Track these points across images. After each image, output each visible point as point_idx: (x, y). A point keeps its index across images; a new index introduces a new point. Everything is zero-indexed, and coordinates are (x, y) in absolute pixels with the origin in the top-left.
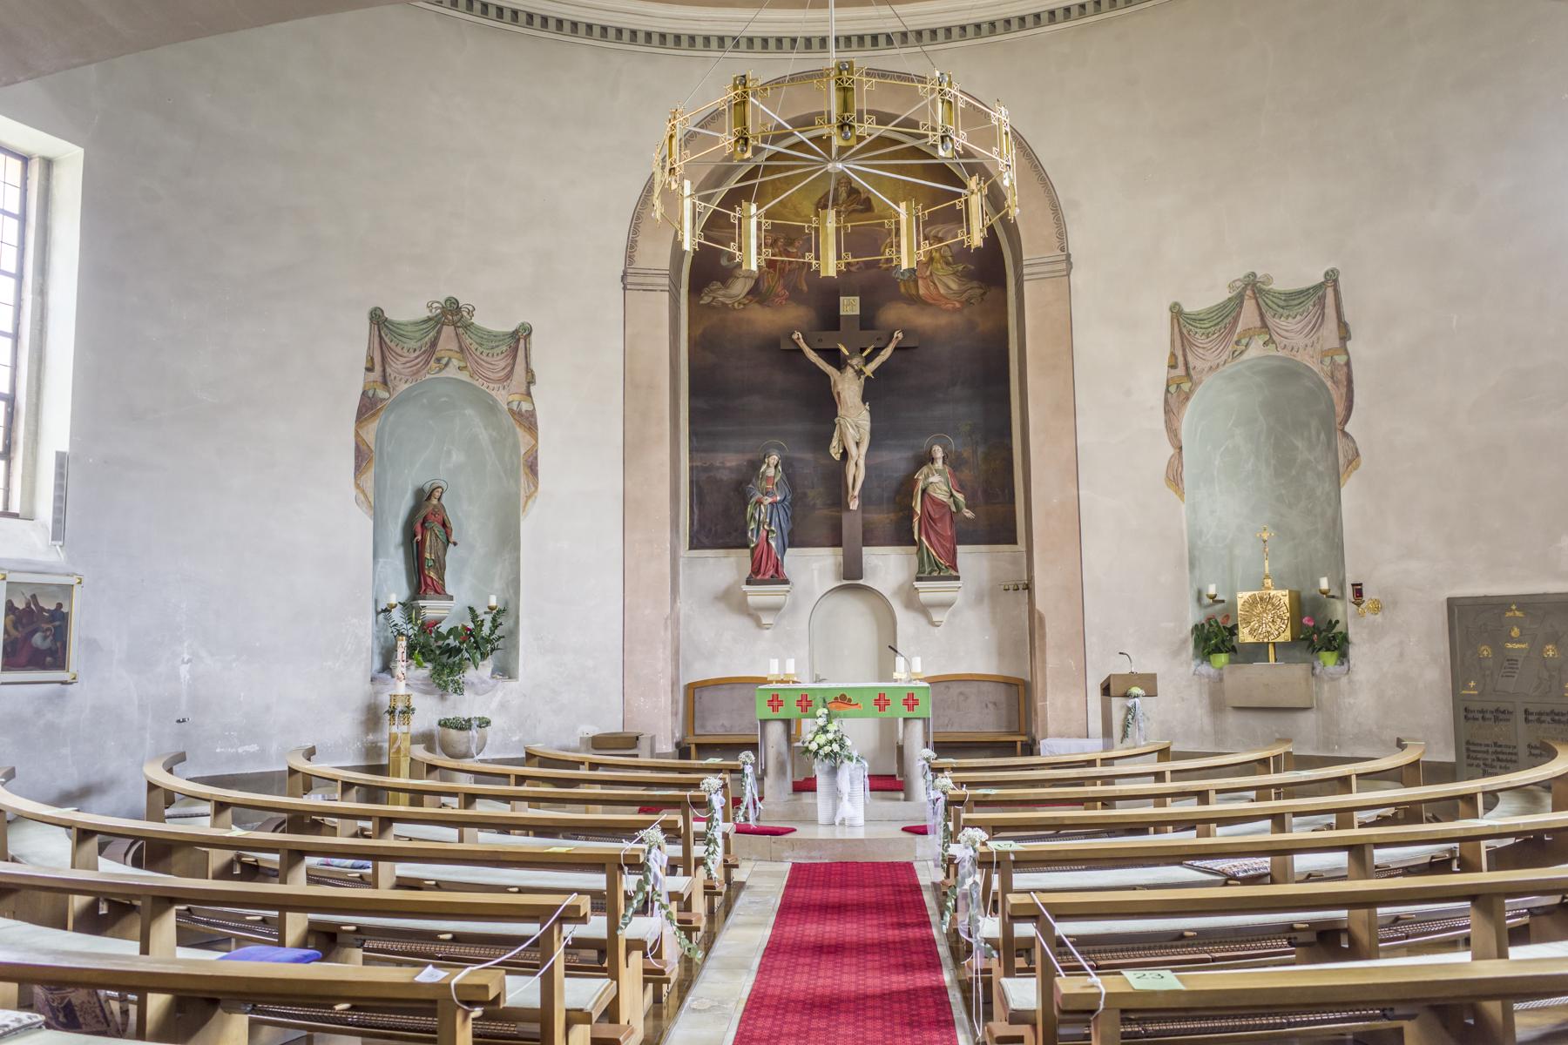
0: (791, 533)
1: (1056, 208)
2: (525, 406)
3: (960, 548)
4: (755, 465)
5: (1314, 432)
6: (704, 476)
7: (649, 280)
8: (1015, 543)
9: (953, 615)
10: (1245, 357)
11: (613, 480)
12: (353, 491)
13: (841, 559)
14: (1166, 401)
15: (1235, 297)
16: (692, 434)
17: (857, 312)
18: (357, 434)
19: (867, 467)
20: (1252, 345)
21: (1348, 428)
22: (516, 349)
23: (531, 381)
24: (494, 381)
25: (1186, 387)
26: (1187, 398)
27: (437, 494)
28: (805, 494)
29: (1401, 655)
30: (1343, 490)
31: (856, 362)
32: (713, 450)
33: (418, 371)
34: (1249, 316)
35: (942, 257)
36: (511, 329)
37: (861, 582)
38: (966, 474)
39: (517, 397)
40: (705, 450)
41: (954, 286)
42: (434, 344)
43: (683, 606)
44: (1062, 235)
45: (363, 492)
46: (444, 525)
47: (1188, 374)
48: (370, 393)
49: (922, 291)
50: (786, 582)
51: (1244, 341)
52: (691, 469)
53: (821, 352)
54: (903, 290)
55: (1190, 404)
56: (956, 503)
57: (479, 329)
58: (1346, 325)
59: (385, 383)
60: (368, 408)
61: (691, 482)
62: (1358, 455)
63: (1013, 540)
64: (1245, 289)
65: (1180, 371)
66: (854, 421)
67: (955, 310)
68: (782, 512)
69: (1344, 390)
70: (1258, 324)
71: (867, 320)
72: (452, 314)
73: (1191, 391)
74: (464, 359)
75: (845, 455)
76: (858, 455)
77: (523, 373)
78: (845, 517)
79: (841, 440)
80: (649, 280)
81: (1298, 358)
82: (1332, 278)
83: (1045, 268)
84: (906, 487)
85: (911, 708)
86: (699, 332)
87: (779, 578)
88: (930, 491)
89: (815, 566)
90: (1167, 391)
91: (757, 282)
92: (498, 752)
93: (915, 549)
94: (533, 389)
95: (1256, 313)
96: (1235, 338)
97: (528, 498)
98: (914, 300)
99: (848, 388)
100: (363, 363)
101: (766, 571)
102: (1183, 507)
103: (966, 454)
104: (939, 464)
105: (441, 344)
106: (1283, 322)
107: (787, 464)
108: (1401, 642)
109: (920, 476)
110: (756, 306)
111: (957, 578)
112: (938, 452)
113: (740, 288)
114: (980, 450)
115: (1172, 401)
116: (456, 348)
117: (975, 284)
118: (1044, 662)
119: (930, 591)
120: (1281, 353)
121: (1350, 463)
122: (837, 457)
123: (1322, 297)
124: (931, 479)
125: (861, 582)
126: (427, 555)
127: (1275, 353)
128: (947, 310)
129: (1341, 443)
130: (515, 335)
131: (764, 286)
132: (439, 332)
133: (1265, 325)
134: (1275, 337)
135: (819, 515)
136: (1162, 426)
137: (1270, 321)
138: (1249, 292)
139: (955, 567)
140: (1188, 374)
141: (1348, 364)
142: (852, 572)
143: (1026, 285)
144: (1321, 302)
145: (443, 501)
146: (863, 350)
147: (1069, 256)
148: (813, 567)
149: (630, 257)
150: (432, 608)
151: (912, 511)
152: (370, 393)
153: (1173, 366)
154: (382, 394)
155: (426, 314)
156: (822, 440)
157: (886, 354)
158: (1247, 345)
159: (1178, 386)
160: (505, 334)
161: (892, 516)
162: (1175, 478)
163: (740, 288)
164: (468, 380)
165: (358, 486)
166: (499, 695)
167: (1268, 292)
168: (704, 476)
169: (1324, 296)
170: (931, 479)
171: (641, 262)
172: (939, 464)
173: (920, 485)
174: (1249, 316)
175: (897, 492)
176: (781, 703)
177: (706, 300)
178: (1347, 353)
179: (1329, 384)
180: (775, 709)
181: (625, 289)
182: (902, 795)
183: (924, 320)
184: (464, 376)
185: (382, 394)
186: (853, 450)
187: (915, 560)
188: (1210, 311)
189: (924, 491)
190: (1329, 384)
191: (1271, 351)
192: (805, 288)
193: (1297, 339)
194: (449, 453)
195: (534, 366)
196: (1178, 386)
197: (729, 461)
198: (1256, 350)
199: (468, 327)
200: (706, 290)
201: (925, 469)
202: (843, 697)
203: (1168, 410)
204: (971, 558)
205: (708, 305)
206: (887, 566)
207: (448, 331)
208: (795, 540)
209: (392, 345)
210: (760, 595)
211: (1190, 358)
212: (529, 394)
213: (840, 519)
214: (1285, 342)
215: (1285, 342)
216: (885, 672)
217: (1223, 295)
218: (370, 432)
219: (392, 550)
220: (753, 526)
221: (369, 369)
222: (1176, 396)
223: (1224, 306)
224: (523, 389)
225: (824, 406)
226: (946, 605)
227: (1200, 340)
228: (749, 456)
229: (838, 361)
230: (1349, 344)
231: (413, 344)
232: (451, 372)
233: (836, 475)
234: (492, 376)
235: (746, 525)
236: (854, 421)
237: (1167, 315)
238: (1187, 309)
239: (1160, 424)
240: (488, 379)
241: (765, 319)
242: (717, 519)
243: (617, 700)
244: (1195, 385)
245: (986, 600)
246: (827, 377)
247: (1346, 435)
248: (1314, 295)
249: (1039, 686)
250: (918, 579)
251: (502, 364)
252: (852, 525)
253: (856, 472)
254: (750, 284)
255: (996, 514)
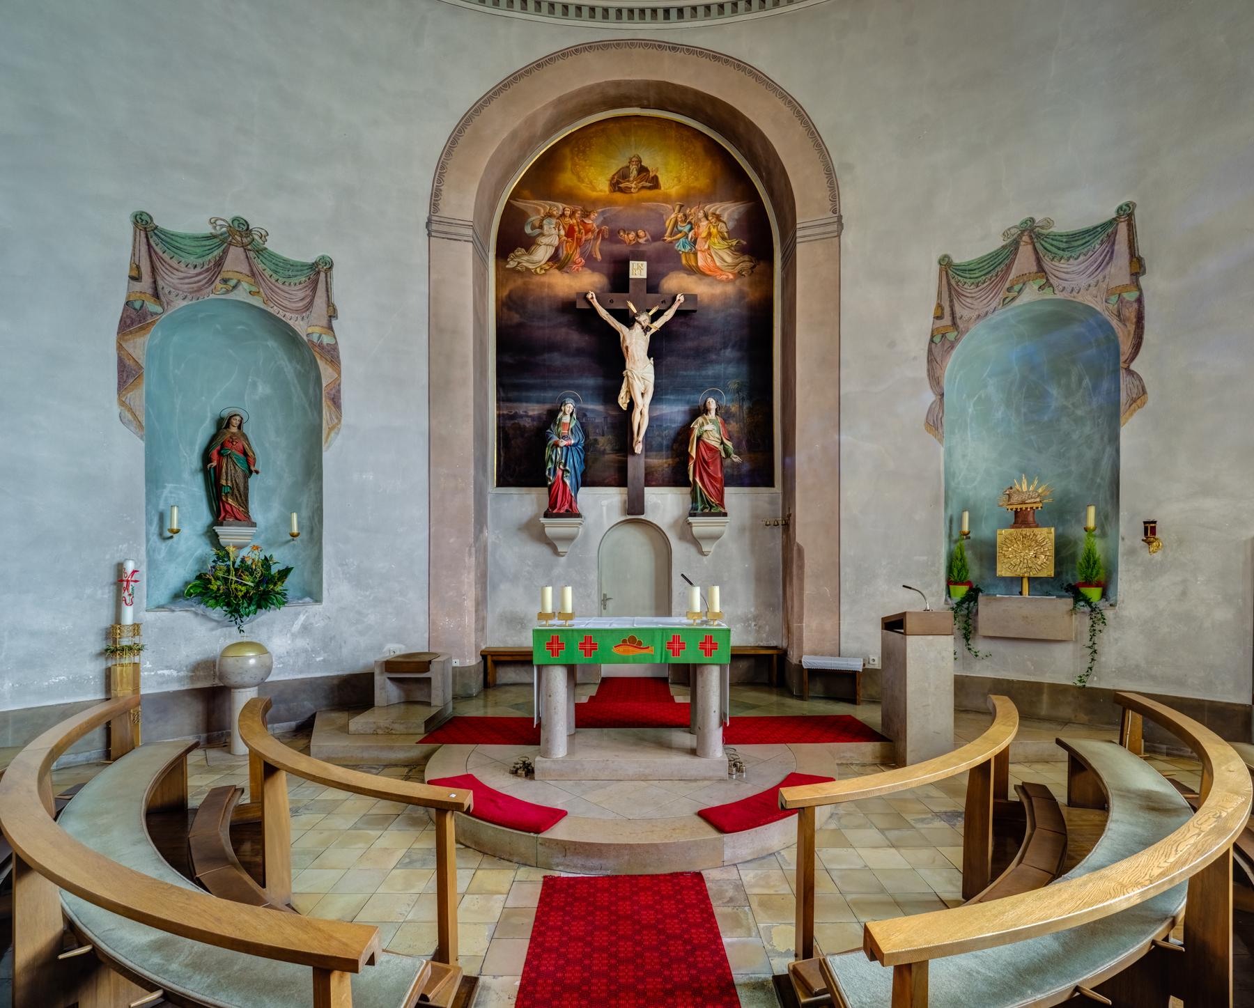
0: (584, 474)
1: (830, 172)
2: (327, 340)
3: (727, 490)
4: (552, 416)
5: (1074, 379)
6: (509, 423)
7: (453, 229)
8: (773, 486)
9: (719, 546)
10: (1017, 302)
11: (422, 422)
12: (116, 409)
13: (625, 497)
14: (930, 351)
15: (1010, 245)
16: (500, 385)
17: (645, 276)
18: (120, 347)
19: (651, 419)
20: (1027, 290)
21: (1133, 367)
22: (316, 282)
23: (332, 314)
24: (291, 310)
25: (951, 336)
26: (952, 347)
27: (235, 422)
28: (596, 440)
29: (1184, 593)
30: (1125, 432)
31: (644, 319)
32: (519, 400)
33: (200, 289)
34: (1025, 261)
35: (719, 232)
36: (311, 259)
37: (642, 517)
38: (734, 426)
39: (317, 330)
40: (509, 400)
41: (729, 259)
42: (219, 263)
43: (490, 535)
44: (835, 197)
45: (130, 410)
46: (245, 453)
47: (954, 324)
48: (137, 305)
49: (700, 263)
50: (579, 516)
51: (1017, 288)
52: (499, 416)
53: (612, 312)
54: (684, 262)
55: (954, 353)
56: (726, 450)
57: (272, 255)
58: (1140, 260)
59: (156, 295)
60: (134, 321)
61: (498, 428)
62: (1144, 392)
63: (770, 484)
64: (1020, 236)
65: (947, 320)
66: (641, 373)
67: (728, 281)
68: (576, 454)
69: (1132, 328)
70: (1034, 269)
71: (652, 285)
72: (239, 234)
73: (957, 340)
74: (257, 283)
75: (631, 405)
76: (643, 404)
77: (324, 306)
78: (630, 460)
79: (629, 392)
80: (453, 229)
81: (1079, 299)
82: (1127, 213)
83: (818, 230)
84: (684, 434)
85: (708, 653)
86: (505, 293)
87: (572, 513)
88: (705, 437)
89: (605, 503)
90: (932, 341)
91: (557, 249)
92: (301, 672)
93: (688, 490)
94: (335, 323)
95: (1033, 258)
96: (1007, 285)
97: (331, 429)
98: (693, 271)
99: (636, 342)
100: (126, 271)
101: (561, 507)
102: (942, 450)
103: (734, 408)
104: (712, 415)
105: (228, 264)
106: (1063, 265)
107: (581, 415)
108: (1184, 581)
109: (696, 426)
110: (557, 271)
111: (725, 515)
112: (712, 404)
113: (542, 254)
114: (746, 405)
115: (936, 350)
116: (246, 270)
117: (746, 258)
118: (801, 589)
119: (701, 525)
120: (1059, 296)
121: (1134, 401)
122: (624, 407)
123: (1118, 235)
124: (706, 427)
125: (642, 517)
126: (223, 482)
127: (1051, 296)
128: (721, 281)
129: (1124, 381)
130: (314, 267)
131: (563, 254)
132: (225, 252)
133: (1041, 269)
134: (1053, 281)
135: (610, 460)
136: (924, 374)
137: (1047, 264)
138: (1026, 238)
139: (723, 506)
140: (954, 324)
141: (1140, 301)
142: (635, 507)
143: (800, 249)
144: (1111, 240)
145: (245, 429)
146: (648, 311)
147: (840, 217)
148: (600, 504)
149: (434, 206)
150: (229, 534)
151: (688, 455)
152: (137, 305)
153: (938, 317)
154: (152, 307)
155: (209, 230)
156: (610, 395)
157: (669, 315)
158: (1020, 291)
159: (943, 335)
160: (303, 265)
161: (670, 461)
162: (934, 423)
163: (542, 254)
164: (262, 306)
165: (122, 403)
166: (302, 618)
167: (1047, 236)
168: (509, 423)
169: (1115, 233)
170: (706, 427)
171: (446, 211)
172: (712, 415)
173: (696, 433)
174: (1025, 261)
175: (675, 440)
176: (561, 646)
177: (512, 264)
178: (1140, 290)
179: (1114, 323)
180: (555, 653)
181: (429, 235)
182: (683, 738)
183: (702, 290)
184: (256, 302)
185: (152, 307)
186: (638, 399)
187: (688, 498)
188: (982, 261)
189: (699, 438)
190: (1114, 323)
191: (1048, 294)
192: (599, 257)
193: (1078, 281)
194: (254, 384)
195: (336, 299)
196: (943, 335)
197: (533, 410)
198: (1030, 294)
199: (260, 251)
200: (512, 255)
201: (700, 420)
202: (632, 639)
203: (931, 359)
204: (734, 497)
205: (514, 270)
206: (665, 503)
207: (235, 253)
208: (587, 480)
209: (166, 257)
210: (555, 527)
211: (957, 308)
212: (330, 328)
213: (626, 462)
214: (1064, 284)
215: (1064, 284)
216: (663, 604)
217: (997, 243)
218: (140, 346)
219: (186, 475)
220: (550, 465)
221: (135, 278)
222: (942, 340)
223: (996, 254)
224: (324, 322)
225: (612, 362)
226: (714, 538)
227: (969, 289)
228: (548, 406)
229: (629, 320)
230: (1143, 281)
231: (192, 259)
232: (241, 295)
233: (623, 420)
234: (286, 303)
235: (545, 465)
236: (641, 373)
237: (935, 268)
238: (956, 261)
239: (922, 371)
240: (285, 308)
241: (566, 284)
242: (522, 458)
243: (422, 620)
244: (961, 333)
245: (747, 534)
246: (616, 335)
247: (1130, 372)
248: (1106, 231)
249: (796, 609)
250: (691, 515)
251: (301, 294)
252: (636, 467)
253: (641, 420)
254: (551, 251)
255: (762, 455)
